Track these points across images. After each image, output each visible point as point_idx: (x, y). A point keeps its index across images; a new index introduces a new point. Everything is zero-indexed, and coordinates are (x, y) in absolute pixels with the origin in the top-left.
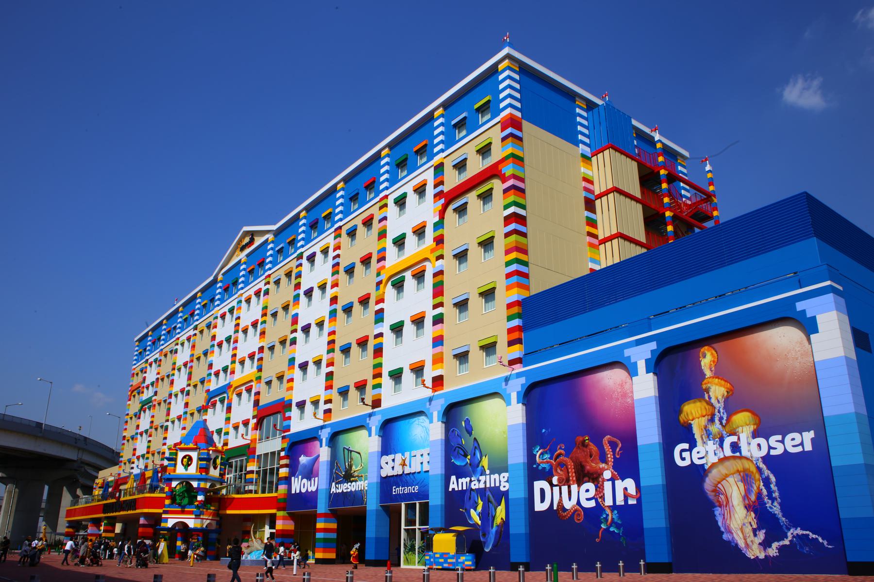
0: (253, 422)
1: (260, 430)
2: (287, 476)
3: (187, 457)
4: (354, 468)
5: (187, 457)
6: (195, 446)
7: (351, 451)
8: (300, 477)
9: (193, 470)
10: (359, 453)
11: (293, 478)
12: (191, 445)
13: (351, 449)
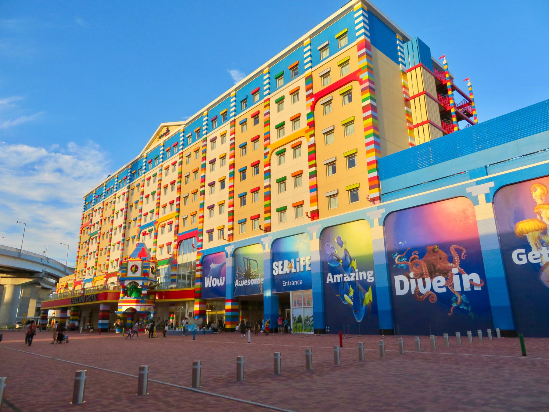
0: (174, 244)
1: (179, 248)
2: (202, 276)
3: (135, 266)
4: (252, 270)
5: (135, 266)
6: (140, 259)
7: (249, 260)
8: (211, 277)
9: (138, 274)
10: (256, 261)
11: (206, 278)
12: (138, 259)
13: (249, 258)
